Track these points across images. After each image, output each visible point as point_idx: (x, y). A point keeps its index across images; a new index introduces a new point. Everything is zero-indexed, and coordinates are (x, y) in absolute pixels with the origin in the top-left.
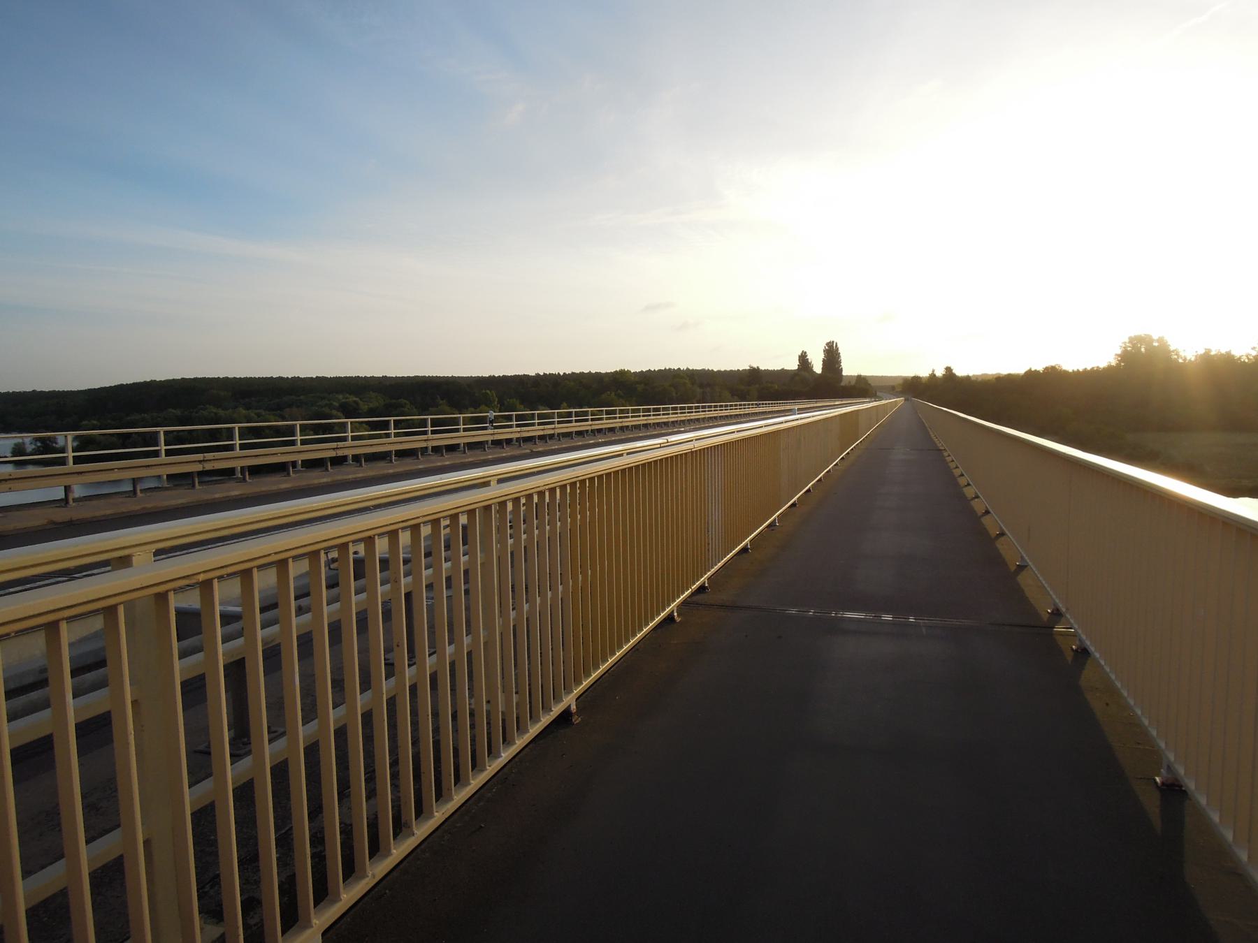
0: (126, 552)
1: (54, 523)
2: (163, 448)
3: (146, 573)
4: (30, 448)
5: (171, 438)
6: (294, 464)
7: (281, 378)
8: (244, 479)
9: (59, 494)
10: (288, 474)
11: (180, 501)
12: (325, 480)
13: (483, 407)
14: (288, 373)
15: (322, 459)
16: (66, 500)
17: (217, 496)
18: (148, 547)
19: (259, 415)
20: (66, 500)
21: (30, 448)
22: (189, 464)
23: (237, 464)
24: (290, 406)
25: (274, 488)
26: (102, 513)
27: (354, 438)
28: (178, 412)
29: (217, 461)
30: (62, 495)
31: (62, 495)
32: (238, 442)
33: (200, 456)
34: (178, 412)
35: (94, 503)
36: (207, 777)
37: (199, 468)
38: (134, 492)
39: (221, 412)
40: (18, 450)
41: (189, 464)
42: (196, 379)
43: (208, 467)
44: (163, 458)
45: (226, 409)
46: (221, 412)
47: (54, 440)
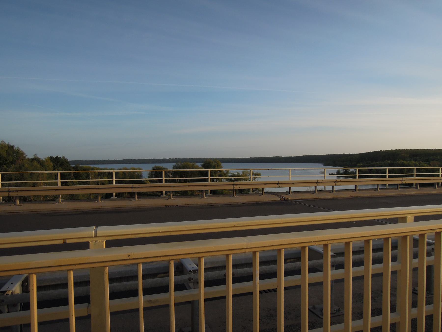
0: (405, 216)
1: (351, 196)
2: (415, 174)
3: (410, 227)
4: (341, 172)
5: (390, 172)
6: (438, 184)
7: (429, 149)
8: (417, 188)
9: (353, 187)
10: (435, 188)
11: (394, 194)
12: (434, 192)
13: (431, 163)
14: (394, 149)
15: (434, 183)
16: (355, 190)
17: (407, 193)
18: (411, 215)
19: (420, 164)
20: (355, 190)
21: (341, 172)
22: (397, 181)
23: (414, 182)
24: (433, 160)
25: (429, 192)
26: (367, 195)
27: (417, 176)
28: (389, 162)
29: (407, 180)
30: (354, 188)
31: (354, 188)
32: (415, 174)
33: (401, 178)
34: (389, 162)
35: (364, 191)
36: (339, 323)
37: (400, 182)
38: (377, 189)
39: (405, 162)
40: (338, 173)
41: (397, 181)
42: (415, 150)
43: (404, 182)
44: (415, 177)
45: (406, 161)
46: (405, 162)
47: (349, 170)
